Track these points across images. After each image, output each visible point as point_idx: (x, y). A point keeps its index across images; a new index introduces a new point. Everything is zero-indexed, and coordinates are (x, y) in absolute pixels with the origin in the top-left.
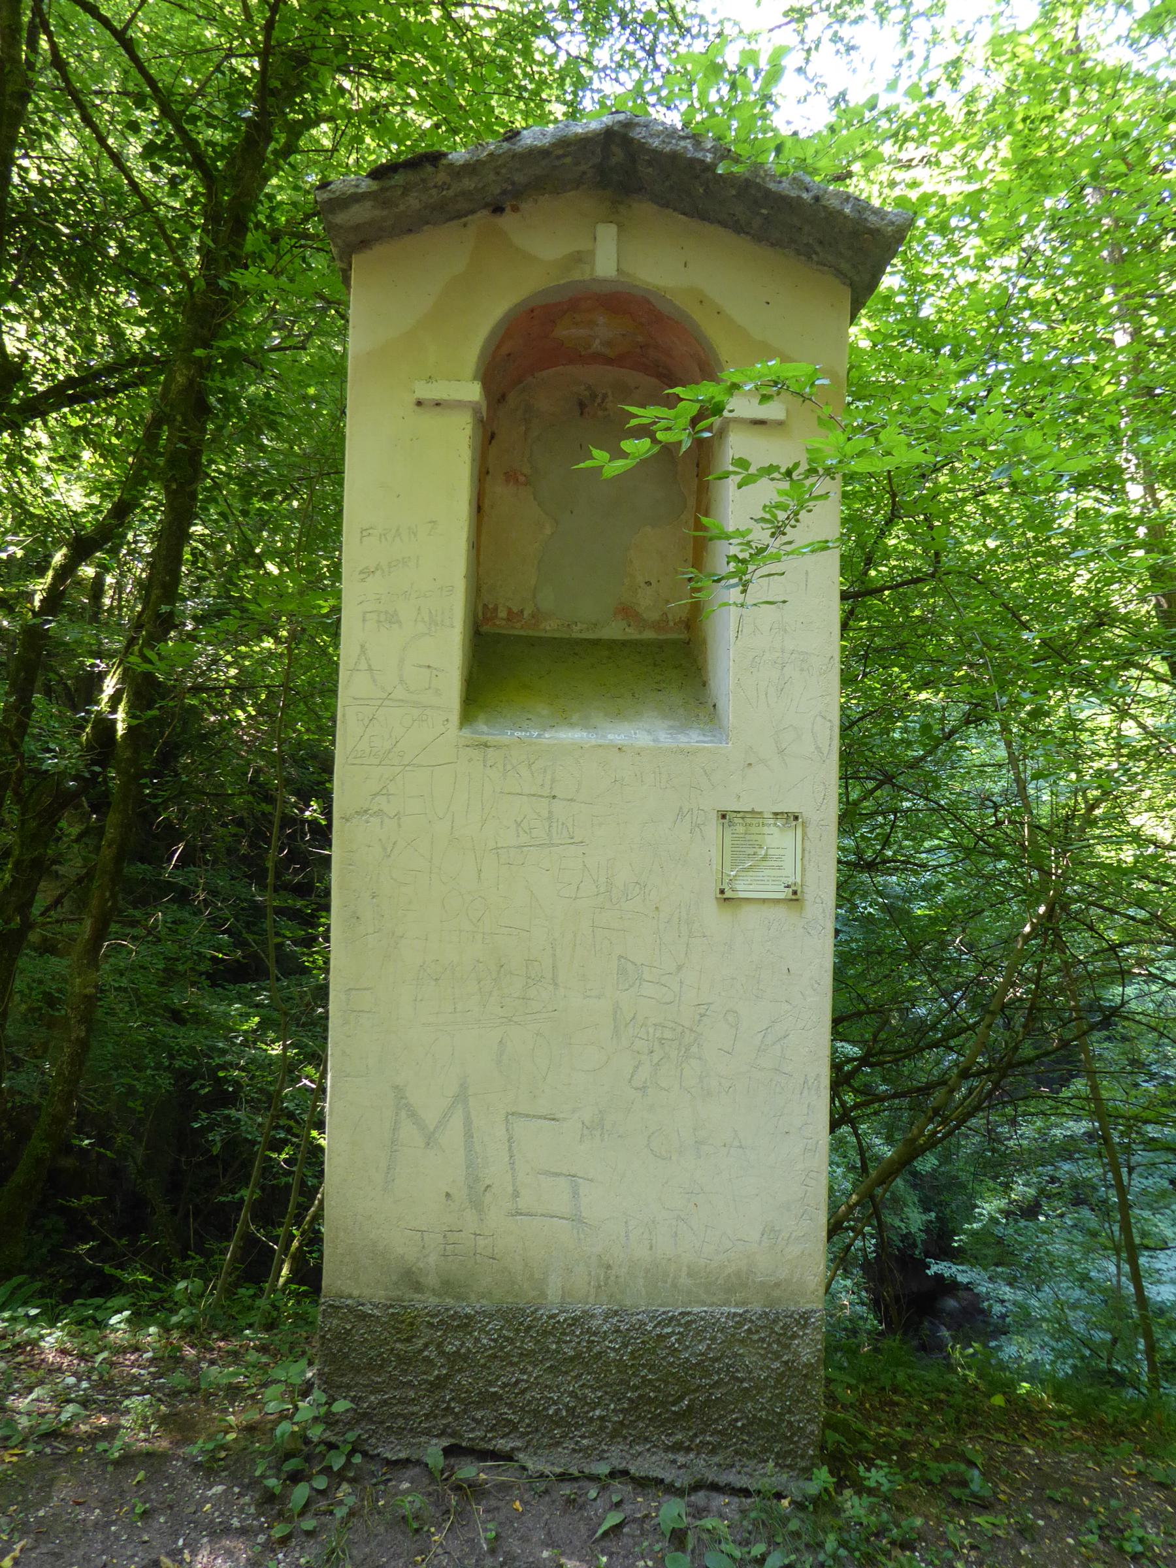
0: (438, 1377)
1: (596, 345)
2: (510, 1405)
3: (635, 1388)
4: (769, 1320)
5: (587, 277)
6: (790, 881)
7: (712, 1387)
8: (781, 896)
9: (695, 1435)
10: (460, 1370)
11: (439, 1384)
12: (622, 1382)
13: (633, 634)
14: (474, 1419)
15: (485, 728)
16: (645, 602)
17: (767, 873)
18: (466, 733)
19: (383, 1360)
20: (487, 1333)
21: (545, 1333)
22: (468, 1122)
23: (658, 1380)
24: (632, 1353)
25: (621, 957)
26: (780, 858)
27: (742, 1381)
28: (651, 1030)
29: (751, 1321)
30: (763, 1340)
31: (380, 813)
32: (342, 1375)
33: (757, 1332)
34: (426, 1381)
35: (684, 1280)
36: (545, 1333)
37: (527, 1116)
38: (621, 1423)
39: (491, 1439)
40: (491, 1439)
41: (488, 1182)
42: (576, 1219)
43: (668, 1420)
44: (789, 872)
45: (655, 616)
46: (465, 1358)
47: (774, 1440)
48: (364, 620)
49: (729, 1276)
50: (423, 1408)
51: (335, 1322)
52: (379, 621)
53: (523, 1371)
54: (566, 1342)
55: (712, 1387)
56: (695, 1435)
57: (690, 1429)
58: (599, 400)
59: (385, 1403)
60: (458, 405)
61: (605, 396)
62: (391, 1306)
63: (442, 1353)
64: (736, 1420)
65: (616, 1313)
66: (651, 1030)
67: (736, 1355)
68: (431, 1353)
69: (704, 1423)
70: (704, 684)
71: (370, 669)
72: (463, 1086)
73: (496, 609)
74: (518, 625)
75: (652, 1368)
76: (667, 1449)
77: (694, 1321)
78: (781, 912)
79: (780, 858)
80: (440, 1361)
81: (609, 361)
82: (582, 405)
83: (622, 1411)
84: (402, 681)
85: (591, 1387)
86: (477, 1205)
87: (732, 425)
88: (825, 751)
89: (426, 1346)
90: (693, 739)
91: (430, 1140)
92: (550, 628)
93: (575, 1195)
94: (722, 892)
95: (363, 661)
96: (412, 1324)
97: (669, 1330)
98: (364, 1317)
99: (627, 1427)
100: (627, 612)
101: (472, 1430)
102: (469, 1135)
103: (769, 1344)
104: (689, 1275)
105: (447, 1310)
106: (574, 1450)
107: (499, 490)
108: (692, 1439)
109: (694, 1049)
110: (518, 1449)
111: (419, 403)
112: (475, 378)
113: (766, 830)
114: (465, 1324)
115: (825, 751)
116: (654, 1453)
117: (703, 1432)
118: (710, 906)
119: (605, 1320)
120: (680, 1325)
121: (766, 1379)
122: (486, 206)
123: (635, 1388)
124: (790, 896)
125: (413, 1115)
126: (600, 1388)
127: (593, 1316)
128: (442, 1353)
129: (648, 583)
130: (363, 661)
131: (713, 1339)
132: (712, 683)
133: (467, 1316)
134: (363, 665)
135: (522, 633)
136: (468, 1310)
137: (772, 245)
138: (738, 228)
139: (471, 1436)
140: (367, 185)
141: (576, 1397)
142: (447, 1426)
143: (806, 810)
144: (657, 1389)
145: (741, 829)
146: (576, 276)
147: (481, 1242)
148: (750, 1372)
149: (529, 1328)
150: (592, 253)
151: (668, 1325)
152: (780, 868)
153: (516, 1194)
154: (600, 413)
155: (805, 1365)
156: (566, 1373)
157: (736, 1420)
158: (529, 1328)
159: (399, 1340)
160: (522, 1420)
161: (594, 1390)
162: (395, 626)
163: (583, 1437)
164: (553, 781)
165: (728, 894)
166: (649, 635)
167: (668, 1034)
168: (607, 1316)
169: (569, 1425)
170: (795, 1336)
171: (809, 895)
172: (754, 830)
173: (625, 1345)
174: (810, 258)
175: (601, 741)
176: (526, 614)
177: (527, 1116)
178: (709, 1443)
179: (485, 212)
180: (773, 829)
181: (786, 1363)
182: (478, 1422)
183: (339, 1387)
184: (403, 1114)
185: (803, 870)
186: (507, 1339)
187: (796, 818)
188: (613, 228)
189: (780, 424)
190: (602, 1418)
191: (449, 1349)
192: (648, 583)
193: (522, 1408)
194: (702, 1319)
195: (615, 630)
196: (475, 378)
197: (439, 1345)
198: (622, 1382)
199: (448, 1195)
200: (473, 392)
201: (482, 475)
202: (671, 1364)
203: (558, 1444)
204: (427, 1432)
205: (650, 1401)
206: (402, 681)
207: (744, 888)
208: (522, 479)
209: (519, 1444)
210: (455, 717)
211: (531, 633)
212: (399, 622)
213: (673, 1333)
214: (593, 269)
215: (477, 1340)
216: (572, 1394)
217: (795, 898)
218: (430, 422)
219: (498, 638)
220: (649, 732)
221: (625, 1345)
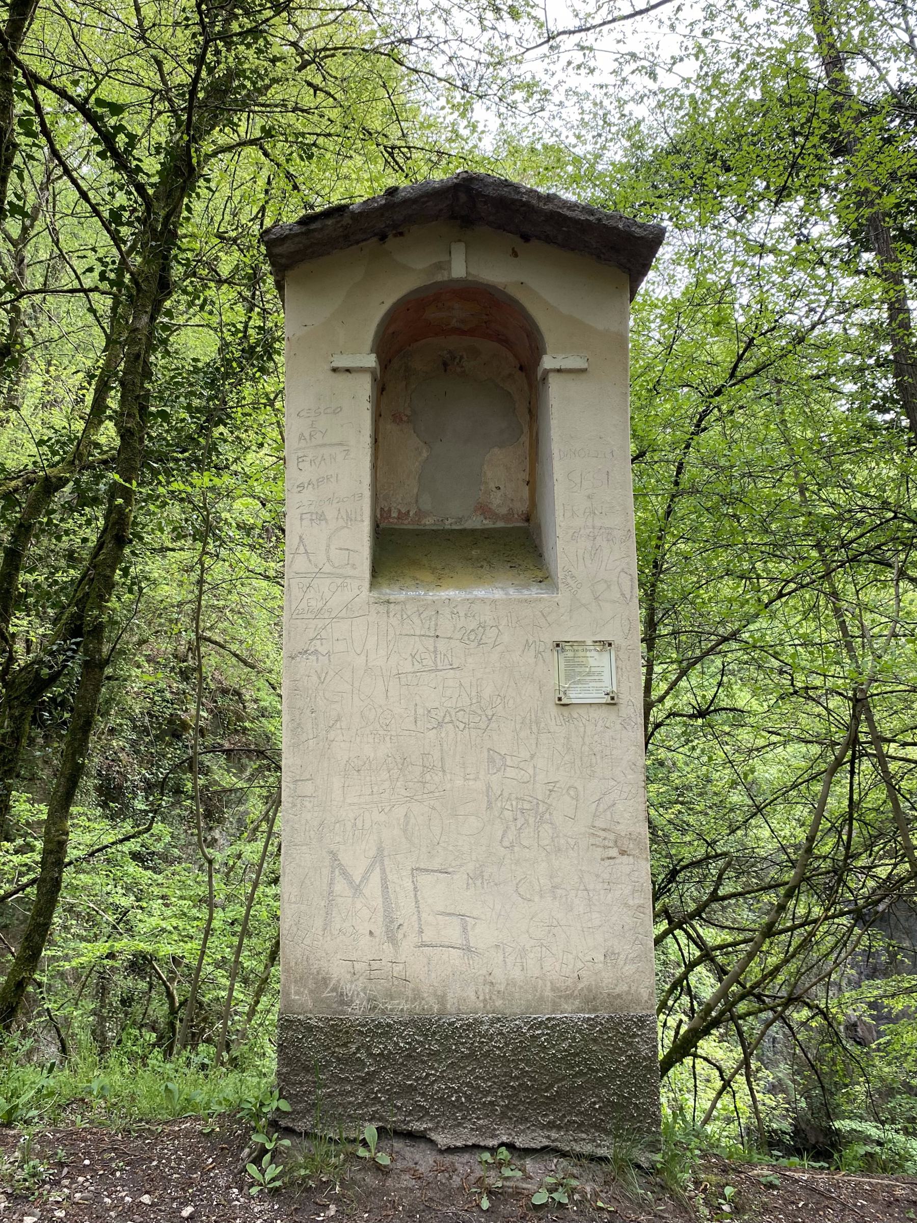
0: (368, 1073)
1: (454, 323)
2: (423, 1095)
3: (517, 1078)
4: (615, 1024)
5: (446, 279)
6: (608, 690)
7: (574, 1076)
8: (604, 701)
9: (564, 1116)
10: (385, 1068)
11: (369, 1078)
12: (505, 1075)
13: (488, 524)
14: (395, 1106)
15: (388, 591)
16: (496, 501)
17: (591, 684)
18: (375, 594)
19: (326, 1061)
20: (403, 1038)
21: (447, 1037)
22: (383, 871)
23: (532, 1072)
24: (512, 1051)
25: (489, 750)
26: (600, 674)
27: (597, 1071)
28: (514, 803)
29: (601, 1024)
30: (610, 1038)
31: (316, 652)
32: (298, 1075)
33: (606, 1033)
34: (359, 1077)
35: (548, 993)
36: (447, 1037)
37: (427, 870)
38: (506, 1106)
39: (409, 1122)
40: (409, 1122)
41: (400, 922)
42: (467, 949)
43: (543, 1103)
44: (607, 683)
45: (504, 511)
46: (387, 1058)
47: (623, 1119)
48: (301, 519)
49: (582, 989)
50: (357, 1098)
51: (291, 1033)
52: (312, 520)
53: (432, 1067)
54: (462, 1044)
55: (574, 1076)
56: (564, 1116)
57: (560, 1110)
58: (457, 360)
59: (329, 1095)
60: (362, 370)
61: (461, 357)
62: (332, 1019)
63: (371, 1055)
64: (595, 1103)
65: (499, 1020)
66: (514, 803)
67: (591, 1051)
68: (362, 1055)
69: (570, 1105)
70: (541, 556)
71: (306, 552)
72: (380, 849)
73: (390, 511)
74: (406, 522)
75: (528, 1062)
76: (543, 1127)
77: (558, 1025)
78: (603, 712)
79: (600, 674)
80: (368, 1062)
81: (463, 333)
82: (445, 364)
83: (508, 1097)
84: (328, 560)
85: (482, 1078)
86: (392, 939)
87: (551, 375)
88: (628, 597)
89: (358, 1049)
90: (534, 592)
91: (357, 889)
92: (429, 522)
93: (465, 929)
94: (560, 699)
95: (302, 548)
96: (347, 1032)
97: (539, 1032)
98: (310, 1029)
99: (511, 1110)
100: (484, 509)
101: (395, 1115)
102: (385, 887)
103: (616, 1042)
104: (553, 990)
105: (373, 1021)
106: (472, 1129)
107: (389, 426)
108: (561, 1119)
109: (547, 816)
110: (430, 1129)
111: (335, 370)
112: (372, 352)
113: (588, 654)
114: (385, 1030)
115: (628, 597)
116: (534, 1131)
117: (570, 1114)
118: (554, 711)
119: (491, 1025)
120: (548, 1028)
121: (615, 1070)
122: (375, 235)
123: (517, 1078)
124: (609, 701)
125: (344, 873)
126: (489, 1079)
127: (482, 1023)
128: (371, 1055)
129: (498, 488)
130: (302, 548)
131: (574, 1038)
132: (546, 555)
133: (388, 1025)
134: (302, 550)
135: (411, 527)
136: (389, 1021)
137: (573, 250)
138: (548, 240)
139: (394, 1120)
140: (297, 229)
141: (472, 1087)
142: (375, 1112)
143: (617, 640)
144: (532, 1079)
145: (570, 654)
146: (441, 277)
147: (398, 968)
148: (602, 1065)
149: (434, 1033)
150: (450, 262)
151: (537, 1029)
152: (600, 681)
153: (421, 932)
154: (459, 370)
155: (644, 1059)
156: (464, 1068)
157: (595, 1103)
158: (434, 1033)
159: (338, 1045)
160: (432, 1106)
161: (485, 1081)
162: (323, 523)
163: (478, 1118)
164: (436, 625)
165: (564, 701)
166: (500, 524)
167: (526, 806)
168: (492, 1023)
169: (468, 1110)
170: (635, 1035)
171: (623, 699)
172: (581, 654)
173: (507, 1045)
174: (599, 257)
175: (468, 596)
176: (411, 514)
177: (427, 870)
178: (575, 1122)
179: (375, 239)
180: (594, 653)
181: (630, 1056)
182: (399, 1108)
183: (294, 1084)
184: (337, 872)
185: (619, 682)
186: (418, 1042)
187: (610, 645)
188: (462, 245)
189: (583, 371)
190: (492, 1103)
191: (376, 1051)
192: (498, 488)
193: (432, 1097)
194: (564, 1023)
195: (476, 522)
196: (372, 352)
197: (368, 1048)
198: (505, 1075)
199: (371, 933)
200: (371, 361)
201: (377, 417)
202: (543, 1059)
203: (460, 1125)
204: (362, 1118)
205: (527, 1089)
206: (328, 560)
207: (575, 696)
208: (405, 418)
209: (430, 1125)
210: (367, 584)
211: (416, 527)
212: (326, 520)
213: (543, 1034)
214: (450, 273)
215: (396, 1044)
216: (468, 1084)
217: (613, 702)
218: (342, 380)
219: (392, 532)
220: (502, 588)
221: (507, 1045)
